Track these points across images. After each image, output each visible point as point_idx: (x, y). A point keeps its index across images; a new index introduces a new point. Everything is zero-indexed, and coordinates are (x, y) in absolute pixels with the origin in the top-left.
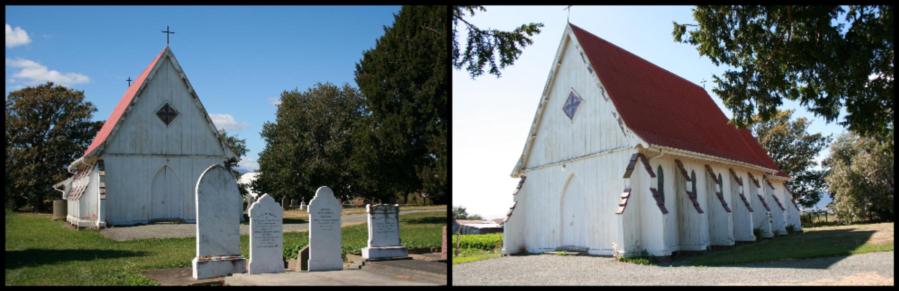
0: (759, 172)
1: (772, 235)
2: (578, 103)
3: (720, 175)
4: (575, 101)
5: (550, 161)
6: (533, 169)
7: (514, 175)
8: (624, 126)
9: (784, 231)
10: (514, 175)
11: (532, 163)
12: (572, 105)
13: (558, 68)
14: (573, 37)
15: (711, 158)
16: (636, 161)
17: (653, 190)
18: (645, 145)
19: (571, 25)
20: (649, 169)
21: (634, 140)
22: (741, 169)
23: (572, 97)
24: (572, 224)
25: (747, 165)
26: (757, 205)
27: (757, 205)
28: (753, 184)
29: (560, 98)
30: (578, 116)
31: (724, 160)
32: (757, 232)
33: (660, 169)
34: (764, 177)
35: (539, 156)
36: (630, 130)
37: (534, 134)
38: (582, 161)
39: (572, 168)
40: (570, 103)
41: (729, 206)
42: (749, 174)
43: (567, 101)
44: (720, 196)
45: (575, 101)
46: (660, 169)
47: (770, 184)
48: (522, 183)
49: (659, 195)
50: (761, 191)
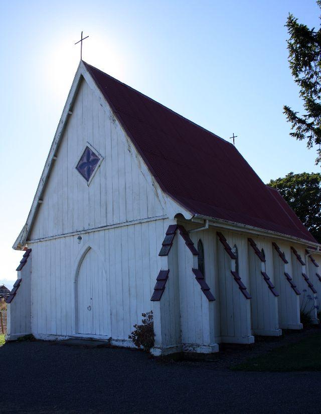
0: (303, 246)
1: (279, 333)
2: (96, 160)
3: (262, 250)
4: (92, 158)
5: (60, 232)
6: (40, 240)
7: (17, 247)
8: (159, 191)
9: (298, 324)
10: (17, 247)
11: (36, 235)
12: (88, 164)
13: (69, 117)
14: (88, 78)
15: (222, 224)
16: (175, 233)
17: (194, 270)
18: (188, 215)
19: (85, 64)
20: (190, 244)
21: (171, 208)
22: (264, 238)
23: (88, 153)
24: (90, 308)
25: (271, 233)
26: (302, 285)
27: (302, 285)
28: (279, 259)
29: (72, 155)
30: (97, 177)
31: (241, 227)
32: (305, 317)
33: (200, 243)
34: (307, 252)
35: (46, 226)
36: (165, 195)
37: (41, 197)
38: (102, 233)
39: (87, 240)
40: (85, 160)
41: (212, 291)
42: (292, 248)
43: (82, 159)
44: (236, 276)
45: (92, 158)
46: (200, 243)
47: (313, 261)
48: (26, 256)
49: (200, 273)
50: (304, 270)
